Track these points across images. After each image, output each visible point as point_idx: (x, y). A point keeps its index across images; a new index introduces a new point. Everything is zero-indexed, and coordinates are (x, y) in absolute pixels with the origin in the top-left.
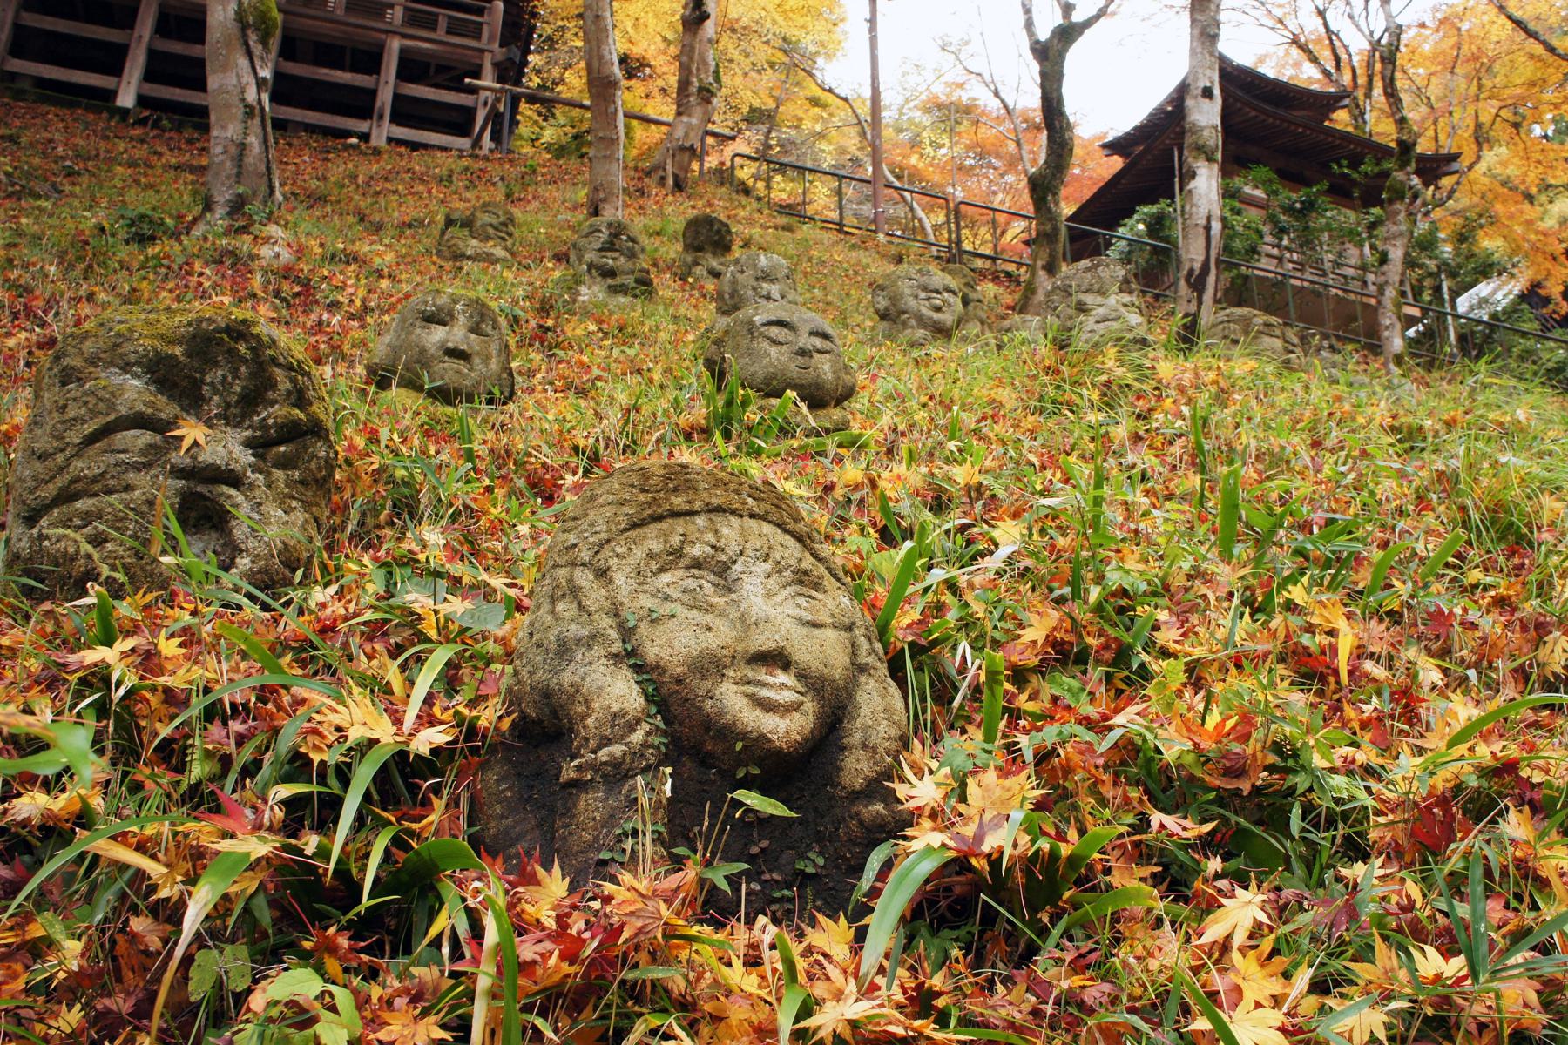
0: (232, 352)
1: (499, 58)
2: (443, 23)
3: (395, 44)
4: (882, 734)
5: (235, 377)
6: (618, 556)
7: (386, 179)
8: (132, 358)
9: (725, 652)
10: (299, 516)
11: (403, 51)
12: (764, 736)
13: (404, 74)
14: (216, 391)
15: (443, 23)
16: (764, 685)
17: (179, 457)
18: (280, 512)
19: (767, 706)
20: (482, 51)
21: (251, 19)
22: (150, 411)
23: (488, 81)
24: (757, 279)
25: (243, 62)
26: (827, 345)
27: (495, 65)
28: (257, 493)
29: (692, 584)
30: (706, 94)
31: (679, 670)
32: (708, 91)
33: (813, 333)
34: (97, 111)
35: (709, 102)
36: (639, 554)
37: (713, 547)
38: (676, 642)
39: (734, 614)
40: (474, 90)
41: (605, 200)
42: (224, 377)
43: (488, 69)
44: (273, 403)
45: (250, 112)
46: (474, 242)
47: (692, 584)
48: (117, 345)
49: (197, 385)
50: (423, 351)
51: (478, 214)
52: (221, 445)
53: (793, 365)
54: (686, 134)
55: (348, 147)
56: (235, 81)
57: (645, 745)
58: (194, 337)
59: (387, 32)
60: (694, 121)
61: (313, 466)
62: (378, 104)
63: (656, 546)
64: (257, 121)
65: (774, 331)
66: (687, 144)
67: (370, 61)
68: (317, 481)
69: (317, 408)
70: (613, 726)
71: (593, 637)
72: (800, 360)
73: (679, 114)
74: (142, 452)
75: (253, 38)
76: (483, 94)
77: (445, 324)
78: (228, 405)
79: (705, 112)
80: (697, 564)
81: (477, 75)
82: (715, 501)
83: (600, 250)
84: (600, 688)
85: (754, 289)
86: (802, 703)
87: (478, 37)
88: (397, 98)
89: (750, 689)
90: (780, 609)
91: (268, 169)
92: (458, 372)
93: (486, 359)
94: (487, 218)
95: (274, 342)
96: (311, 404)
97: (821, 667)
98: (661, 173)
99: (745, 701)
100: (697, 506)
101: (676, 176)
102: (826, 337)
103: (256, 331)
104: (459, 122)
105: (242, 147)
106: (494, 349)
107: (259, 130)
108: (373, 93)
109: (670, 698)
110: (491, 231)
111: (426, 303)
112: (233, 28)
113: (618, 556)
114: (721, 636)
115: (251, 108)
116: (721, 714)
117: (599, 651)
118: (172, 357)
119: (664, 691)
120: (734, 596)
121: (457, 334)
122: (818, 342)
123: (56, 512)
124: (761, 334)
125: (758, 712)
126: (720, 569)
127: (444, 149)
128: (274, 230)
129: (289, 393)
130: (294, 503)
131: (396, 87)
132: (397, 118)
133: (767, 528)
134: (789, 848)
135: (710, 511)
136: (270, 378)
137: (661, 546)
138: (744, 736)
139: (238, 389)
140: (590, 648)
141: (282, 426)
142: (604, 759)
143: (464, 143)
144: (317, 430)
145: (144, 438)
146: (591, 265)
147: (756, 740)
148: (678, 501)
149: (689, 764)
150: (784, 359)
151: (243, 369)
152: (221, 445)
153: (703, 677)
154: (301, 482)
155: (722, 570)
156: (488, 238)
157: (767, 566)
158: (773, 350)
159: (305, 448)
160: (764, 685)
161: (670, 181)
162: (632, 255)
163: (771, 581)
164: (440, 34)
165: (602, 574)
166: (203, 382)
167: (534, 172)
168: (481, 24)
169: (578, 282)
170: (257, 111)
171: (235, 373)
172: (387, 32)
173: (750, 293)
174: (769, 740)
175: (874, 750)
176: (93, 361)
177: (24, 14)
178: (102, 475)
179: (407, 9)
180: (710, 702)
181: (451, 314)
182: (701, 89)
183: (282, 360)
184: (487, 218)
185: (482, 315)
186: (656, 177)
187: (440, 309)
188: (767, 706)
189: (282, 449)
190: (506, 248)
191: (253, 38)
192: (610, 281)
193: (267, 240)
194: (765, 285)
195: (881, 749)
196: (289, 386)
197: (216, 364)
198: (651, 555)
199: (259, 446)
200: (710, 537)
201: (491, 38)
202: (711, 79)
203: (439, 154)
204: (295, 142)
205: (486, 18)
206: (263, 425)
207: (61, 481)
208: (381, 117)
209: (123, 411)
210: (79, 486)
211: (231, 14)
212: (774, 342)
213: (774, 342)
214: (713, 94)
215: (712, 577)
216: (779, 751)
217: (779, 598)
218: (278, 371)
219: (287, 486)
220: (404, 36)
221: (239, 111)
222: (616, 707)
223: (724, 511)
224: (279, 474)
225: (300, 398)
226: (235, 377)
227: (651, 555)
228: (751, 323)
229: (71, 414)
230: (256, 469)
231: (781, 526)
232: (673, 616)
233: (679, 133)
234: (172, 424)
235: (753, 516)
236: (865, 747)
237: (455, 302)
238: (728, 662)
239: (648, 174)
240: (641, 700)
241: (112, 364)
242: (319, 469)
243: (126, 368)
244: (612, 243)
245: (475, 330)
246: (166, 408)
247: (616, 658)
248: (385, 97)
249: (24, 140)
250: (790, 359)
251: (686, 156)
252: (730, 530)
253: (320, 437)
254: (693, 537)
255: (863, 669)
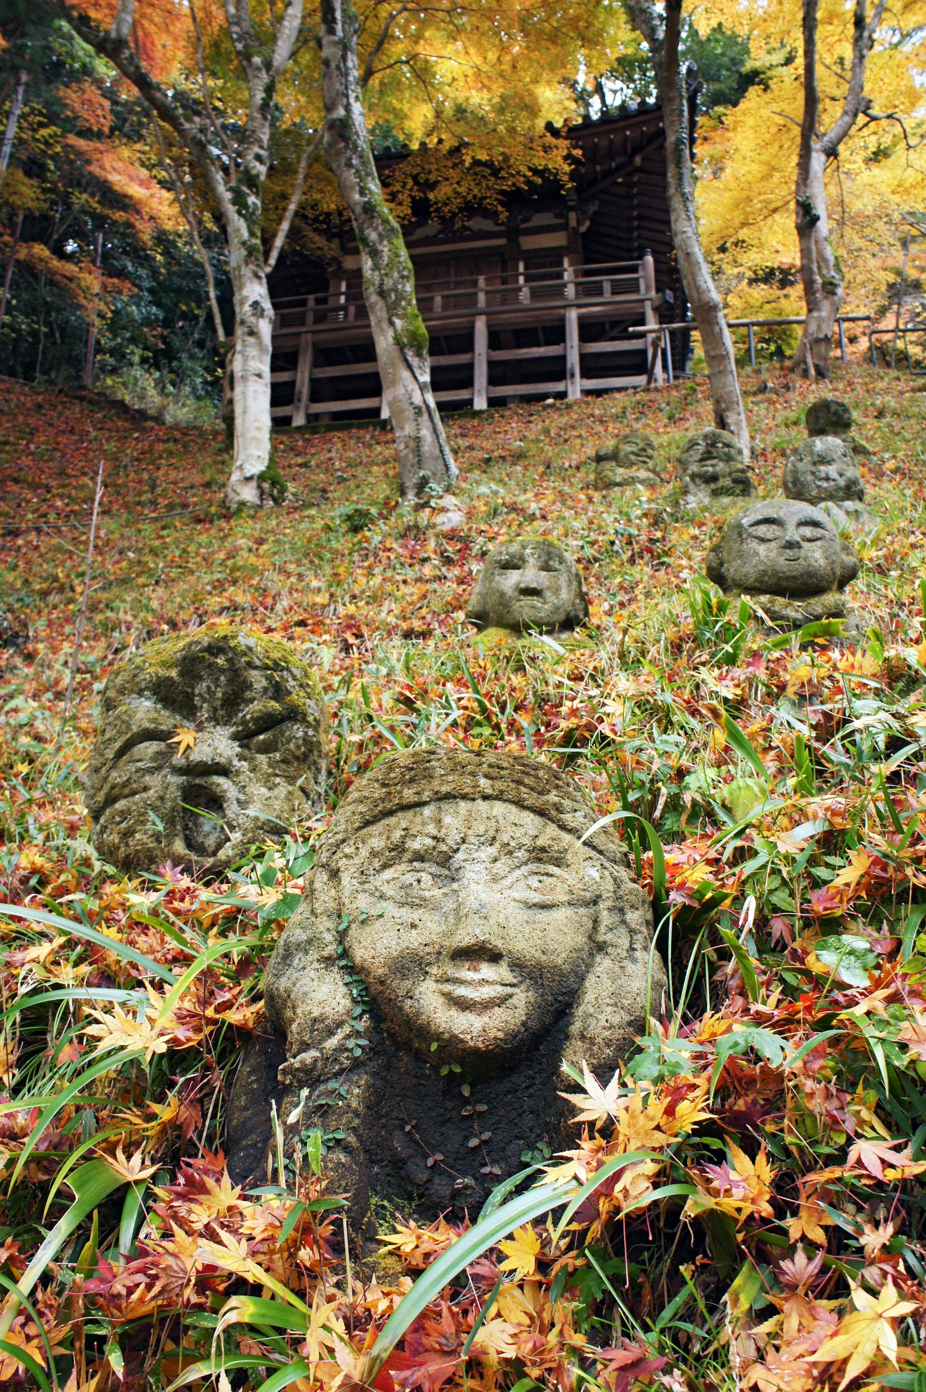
0: (211, 666)
1: (657, 303)
2: (607, 287)
3: (573, 316)
4: (603, 1023)
5: (217, 686)
6: (346, 856)
7: (573, 427)
8: (143, 685)
9: (427, 949)
10: (283, 789)
11: (581, 318)
12: (456, 1036)
13: (585, 337)
14: (204, 700)
15: (607, 287)
16: (462, 982)
17: (178, 759)
18: (264, 790)
19: (463, 1005)
20: (642, 301)
21: (405, 340)
22: (153, 726)
23: (652, 324)
24: (814, 464)
25: (406, 374)
26: (818, 532)
27: (655, 309)
28: (241, 778)
29: (410, 878)
30: (830, 288)
31: (380, 971)
32: (831, 284)
33: (801, 524)
34: (364, 427)
35: (834, 293)
36: (364, 852)
37: (434, 838)
38: (379, 944)
39: (450, 904)
40: (642, 335)
41: (727, 409)
42: (209, 687)
43: (650, 316)
44: (252, 701)
45: (418, 411)
46: (621, 471)
47: (410, 878)
48: (135, 676)
49: (190, 697)
50: (502, 594)
51: (621, 446)
52: (215, 744)
53: (782, 561)
54: (819, 327)
55: (545, 408)
56: (402, 391)
57: (341, 1049)
58: (185, 658)
59: (564, 307)
60: (824, 314)
61: (292, 746)
62: (569, 366)
63: (377, 843)
64: (425, 416)
65: (762, 530)
66: (821, 336)
67: (557, 334)
68: (297, 758)
69: (297, 697)
70: (312, 1031)
71: (310, 942)
72: (790, 553)
73: (810, 311)
74: (153, 759)
75: (410, 354)
76: (650, 337)
77: (518, 568)
78: (215, 710)
79: (833, 304)
80: (419, 857)
81: (642, 322)
82: (445, 789)
83: (701, 461)
84: (305, 994)
85: (813, 473)
86: (511, 996)
87: (637, 290)
88: (583, 357)
89: (447, 988)
90: (507, 893)
91: (441, 451)
92: (533, 607)
93: (557, 591)
94: (628, 448)
95: (250, 649)
96: (290, 693)
97: (538, 954)
98: (802, 366)
99: (442, 1000)
100: (425, 798)
101: (817, 367)
102: (816, 524)
103: (232, 643)
104: (637, 364)
105: (418, 439)
106: (563, 581)
107: (428, 424)
108: (563, 358)
109: (378, 1002)
110: (633, 458)
111: (500, 553)
112: (394, 351)
113: (346, 856)
114: (430, 930)
115: (419, 408)
116: (418, 1014)
117: (313, 955)
118: (170, 679)
119: (372, 990)
120: (455, 886)
121: (531, 575)
122: (808, 531)
123: (108, 811)
124: (751, 536)
125: (454, 1012)
126: (443, 861)
127: (620, 390)
128: (449, 501)
129: (265, 690)
130: (278, 780)
131: (580, 348)
132: (585, 374)
133: (499, 808)
134: (517, 1138)
135: (439, 799)
136: (244, 682)
137: (382, 844)
138: (438, 1037)
139: (219, 695)
140: (306, 952)
141: (259, 718)
142: (297, 1065)
143: (641, 380)
144: (294, 714)
145: (150, 748)
146: (693, 477)
147: (449, 1041)
148: (409, 794)
149: (405, 1059)
150: (772, 555)
151: (222, 678)
152: (215, 744)
153: (404, 977)
154: (284, 761)
155: (445, 860)
156: (632, 464)
157: (493, 851)
158: (762, 549)
159: (282, 733)
160: (462, 982)
161: (812, 372)
162: (729, 459)
163: (498, 864)
164: (607, 296)
165: (335, 874)
166: (193, 694)
167: (695, 391)
168: (637, 279)
169: (686, 492)
170: (424, 409)
171: (216, 681)
172: (564, 307)
173: (810, 478)
174: (462, 1041)
175: (592, 1041)
176: (122, 691)
177: (315, 370)
178: (128, 780)
179: (577, 284)
180: (409, 1002)
181: (522, 558)
182: (824, 285)
183: (258, 663)
184: (628, 448)
185: (549, 554)
186: (799, 371)
187: (512, 556)
188: (463, 1005)
189: (262, 737)
190: (649, 470)
191: (410, 354)
192: (713, 486)
193: (444, 510)
194: (822, 468)
195: (599, 1040)
196: (264, 683)
197: (201, 678)
198: (374, 854)
199: (243, 738)
200: (431, 829)
201: (648, 289)
202: (833, 273)
203: (617, 395)
204: (507, 413)
205: (641, 273)
206: (244, 722)
207: (106, 788)
208: (573, 376)
209: (135, 729)
210: (116, 791)
211: (391, 340)
212: (763, 540)
213: (763, 540)
214: (835, 286)
215: (435, 869)
216: (476, 1051)
217: (507, 882)
218: (254, 673)
219: (270, 766)
220: (579, 306)
221: (410, 413)
222: (316, 1013)
223: (455, 797)
224: (262, 759)
225: (278, 691)
226: (217, 686)
227: (374, 854)
228: (739, 526)
229: (107, 736)
230: (241, 758)
231: (519, 804)
232: (381, 916)
233: (813, 327)
234: (169, 734)
235: (486, 798)
236: (583, 1037)
237: (524, 547)
238: (432, 958)
239: (792, 370)
240: (347, 1003)
241: (132, 691)
242: (298, 747)
243: (140, 693)
244: (709, 452)
245: (546, 568)
246: (167, 719)
247: (328, 961)
248: (574, 360)
249: (313, 463)
250: (779, 554)
251: (822, 348)
252: (453, 819)
253: (296, 721)
254: (413, 831)
255: (601, 947)
